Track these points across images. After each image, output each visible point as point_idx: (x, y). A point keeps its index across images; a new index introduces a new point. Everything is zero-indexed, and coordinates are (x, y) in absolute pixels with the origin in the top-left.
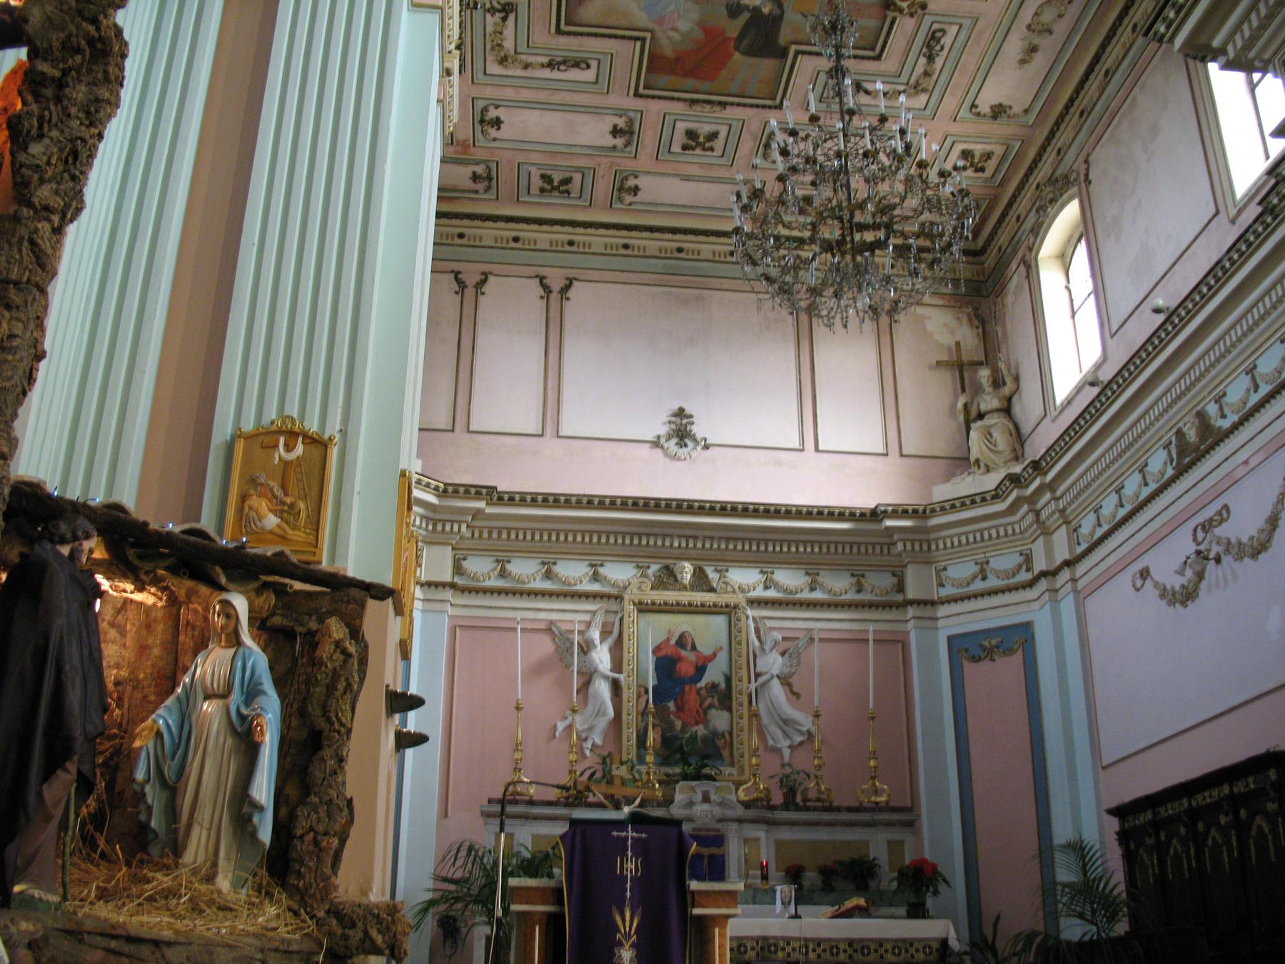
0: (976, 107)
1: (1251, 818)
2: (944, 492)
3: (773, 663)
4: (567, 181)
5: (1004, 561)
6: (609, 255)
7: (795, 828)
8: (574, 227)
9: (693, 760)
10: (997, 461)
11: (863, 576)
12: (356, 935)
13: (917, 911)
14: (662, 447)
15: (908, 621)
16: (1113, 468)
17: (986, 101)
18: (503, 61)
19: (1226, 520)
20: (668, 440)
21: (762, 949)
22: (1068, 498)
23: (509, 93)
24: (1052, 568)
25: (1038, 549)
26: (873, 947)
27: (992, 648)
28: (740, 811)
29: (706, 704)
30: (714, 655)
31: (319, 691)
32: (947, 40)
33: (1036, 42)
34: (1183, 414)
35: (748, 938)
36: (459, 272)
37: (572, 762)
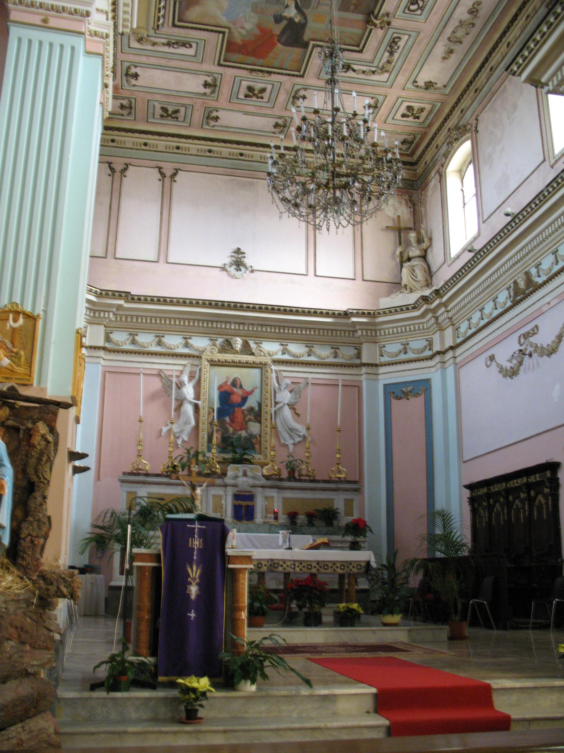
0: (416, 82)
1: (536, 495)
2: (386, 302)
3: (285, 397)
4: (177, 112)
5: (417, 344)
6: (201, 156)
7: (294, 491)
8: (180, 138)
9: (238, 450)
10: (416, 286)
11: (338, 348)
12: (53, 589)
13: (355, 546)
14: (227, 271)
15: (362, 375)
16: (479, 297)
17: (422, 79)
18: (140, 40)
19: (536, 334)
20: (230, 266)
21: (271, 565)
22: (454, 311)
23: (144, 59)
24: (443, 350)
25: (436, 338)
26: (330, 565)
27: (408, 392)
28: (263, 482)
29: (247, 418)
30: (253, 391)
31: (32, 461)
32: (401, 44)
33: (453, 47)
34: (518, 272)
35: (262, 560)
36: (112, 163)
37: (170, 452)
